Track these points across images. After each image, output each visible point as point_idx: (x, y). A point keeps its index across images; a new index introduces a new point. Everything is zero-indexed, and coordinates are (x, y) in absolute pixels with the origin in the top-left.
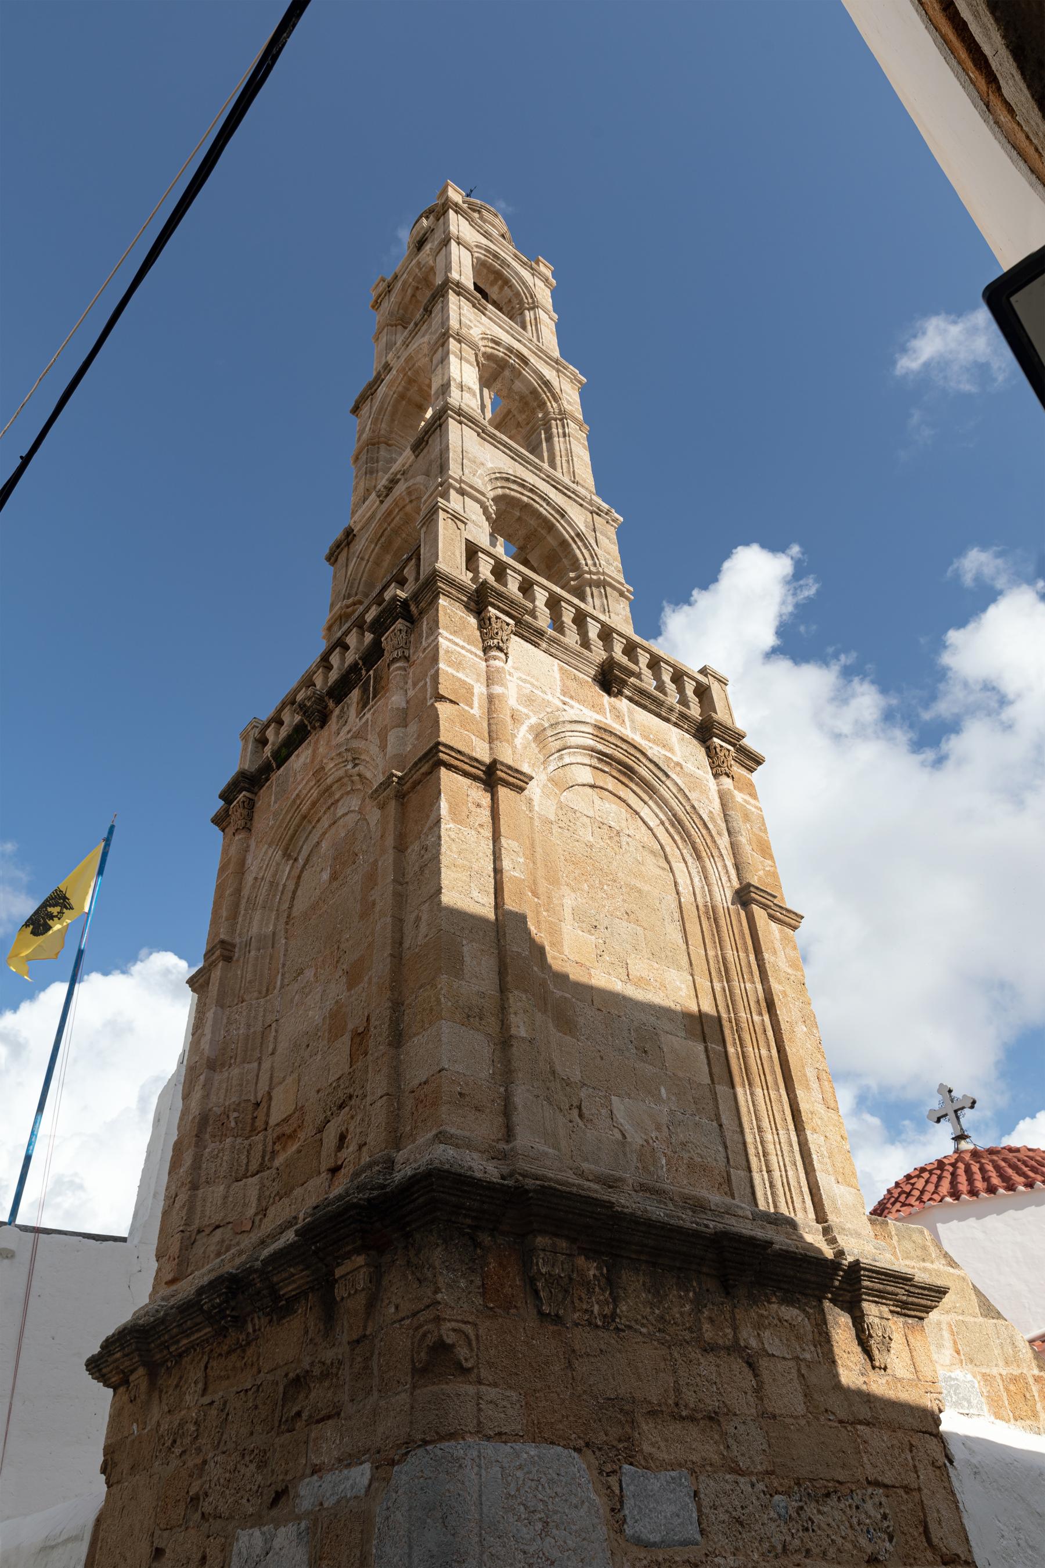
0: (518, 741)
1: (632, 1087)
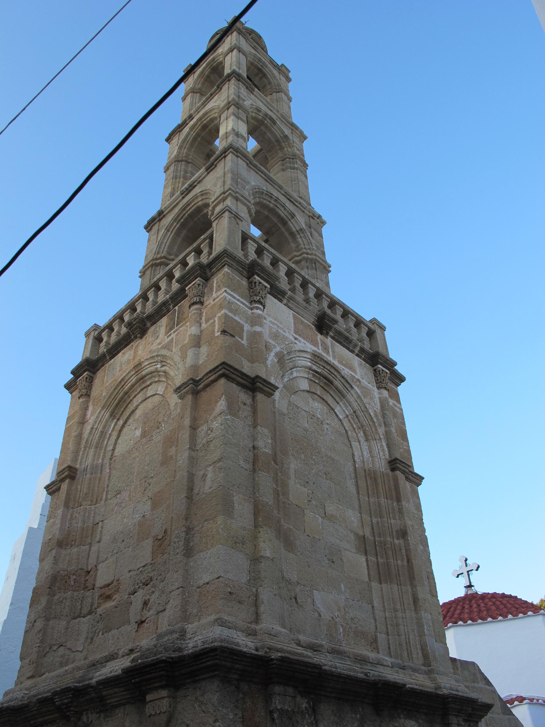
0: (269, 362)
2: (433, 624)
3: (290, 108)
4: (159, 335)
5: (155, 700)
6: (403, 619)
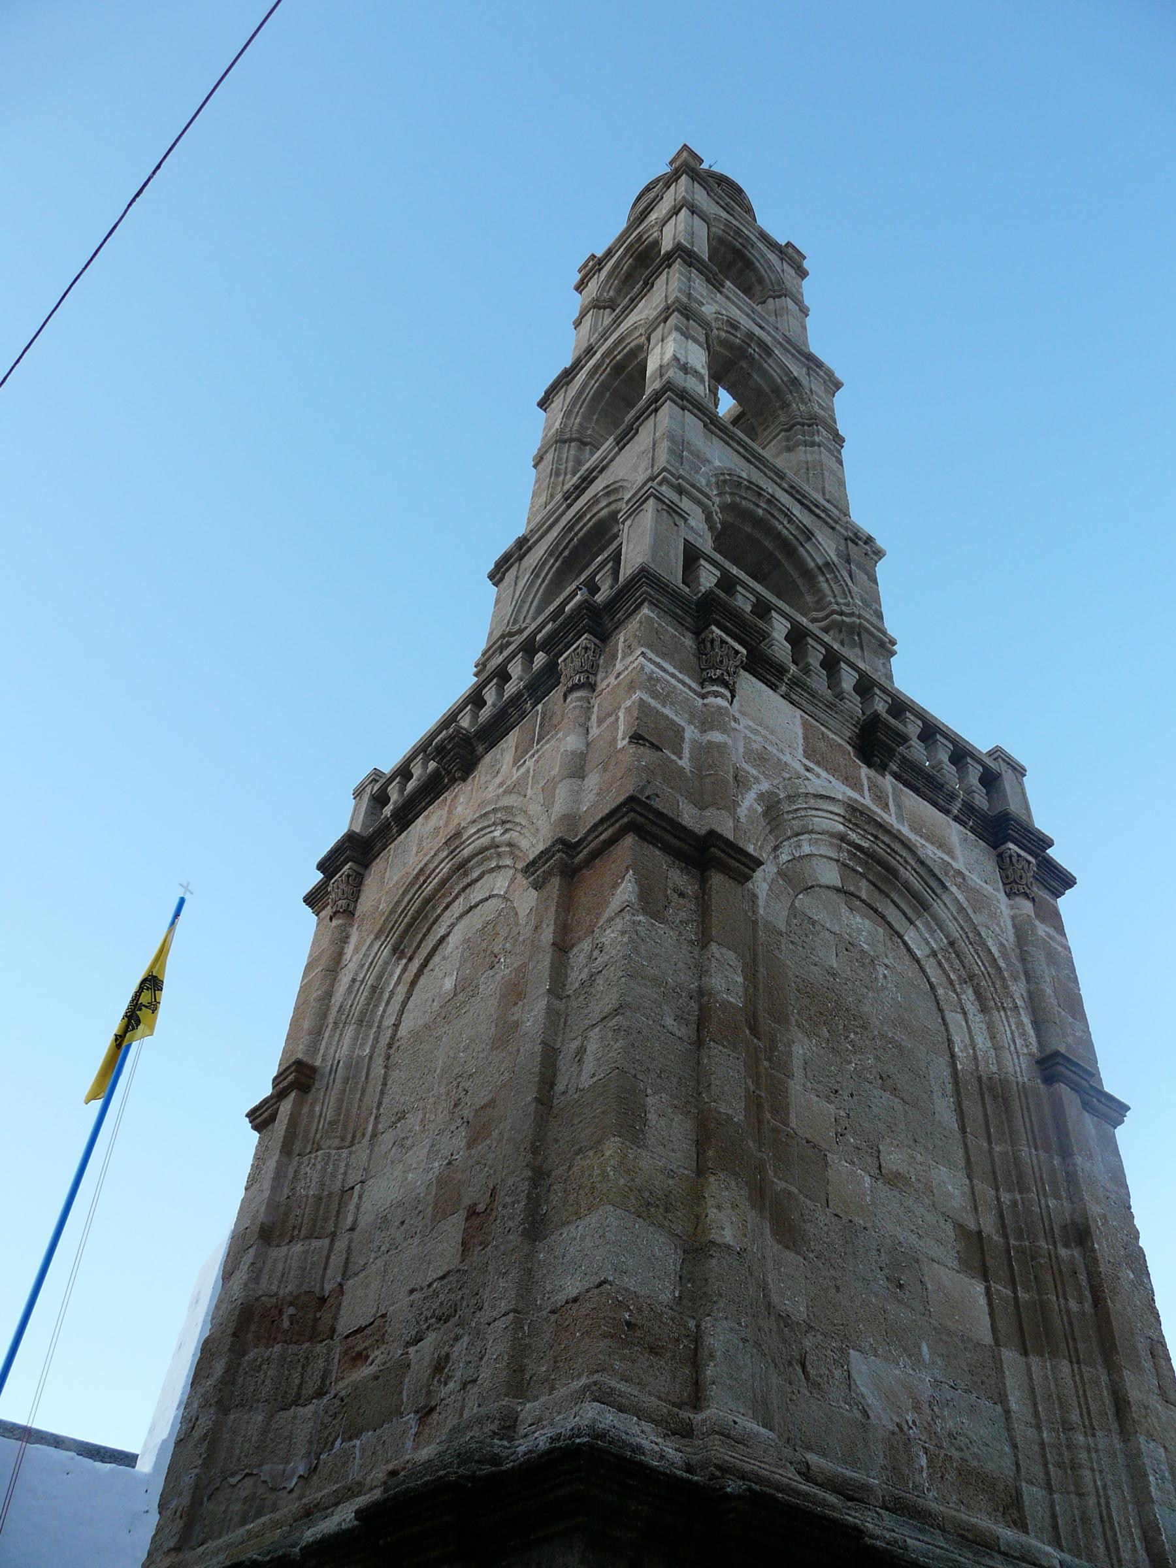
0: (742, 812)
1: (879, 1339)
4: (502, 765)
6: (1089, 1451)
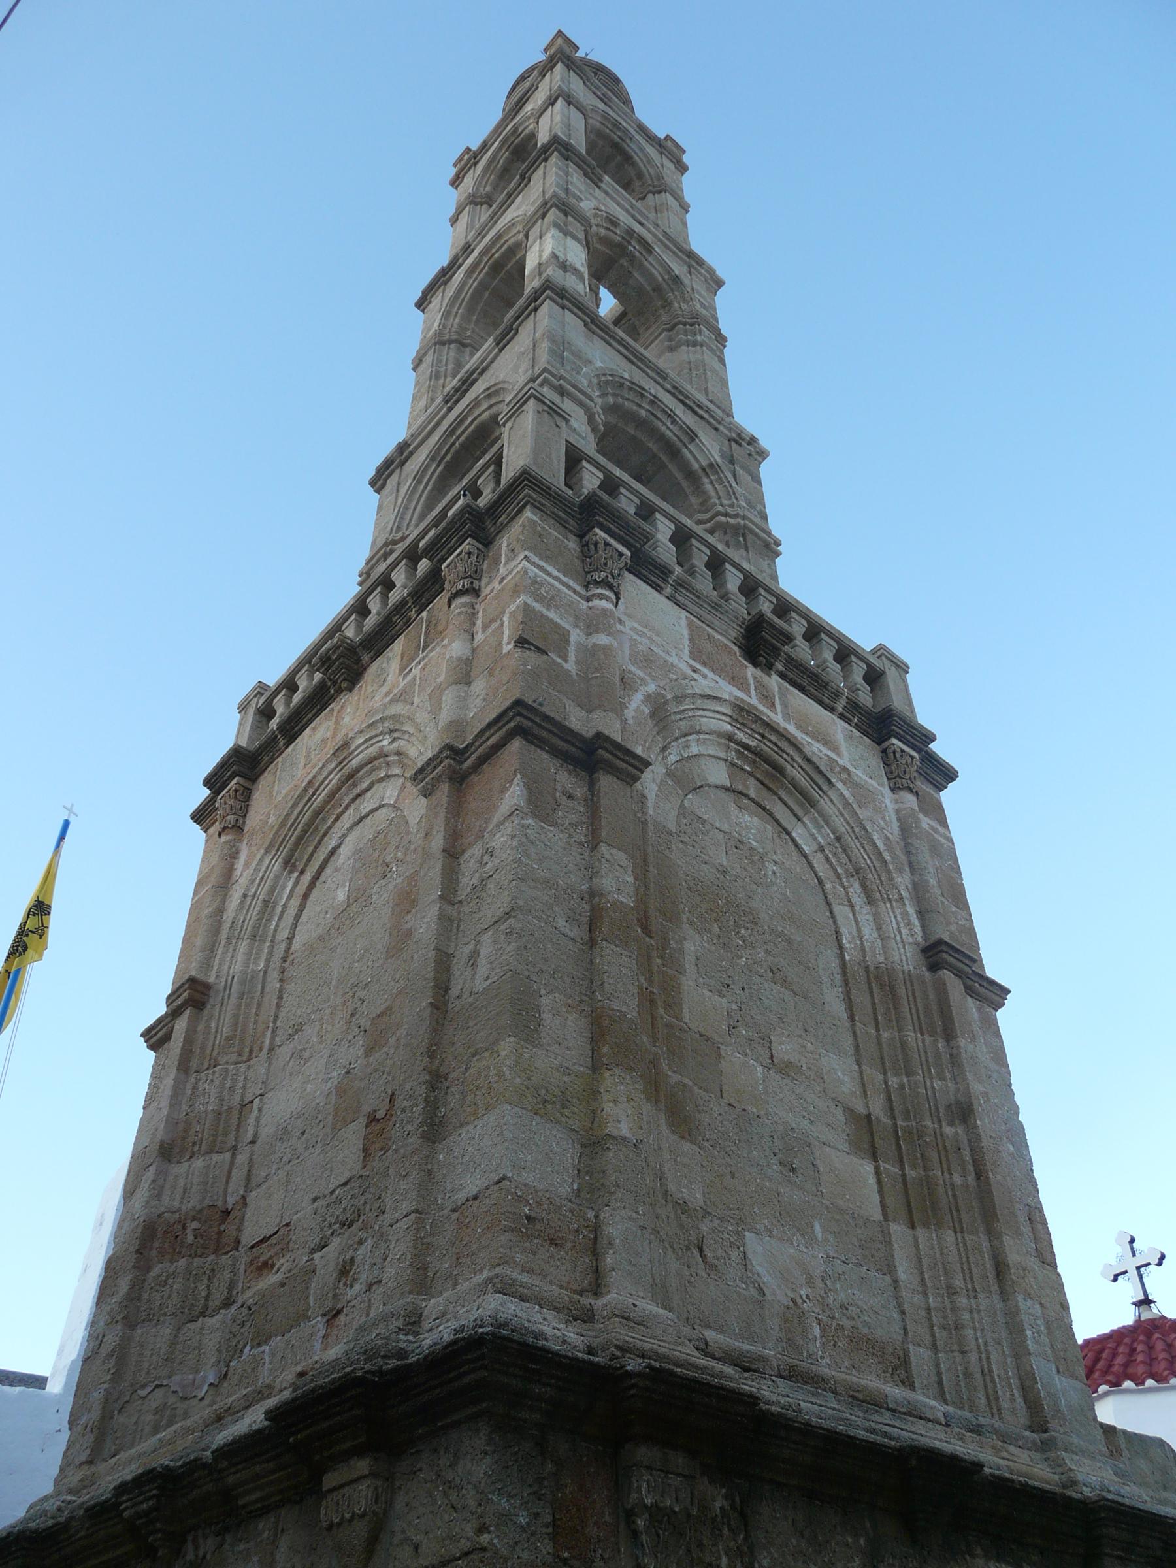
0: (629, 713)
2: (1048, 1328)
3: (685, 225)
4: (388, 674)
5: (342, 1486)
6: (971, 1312)
